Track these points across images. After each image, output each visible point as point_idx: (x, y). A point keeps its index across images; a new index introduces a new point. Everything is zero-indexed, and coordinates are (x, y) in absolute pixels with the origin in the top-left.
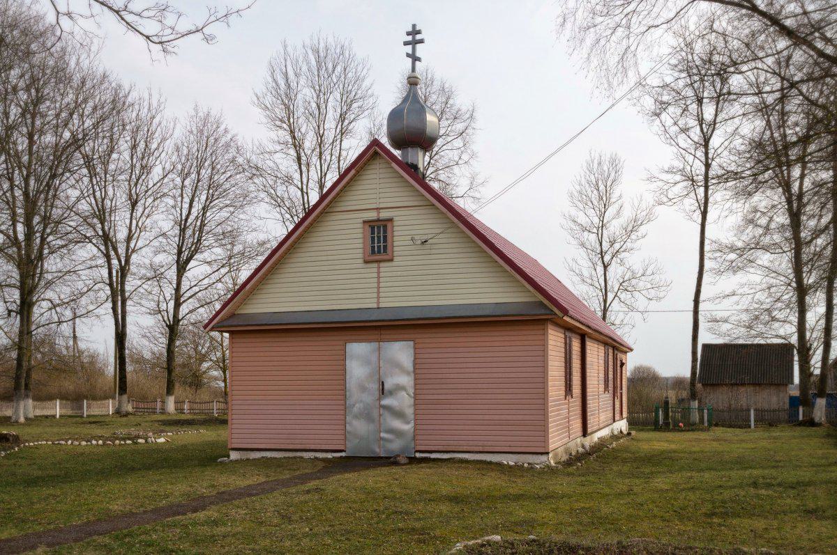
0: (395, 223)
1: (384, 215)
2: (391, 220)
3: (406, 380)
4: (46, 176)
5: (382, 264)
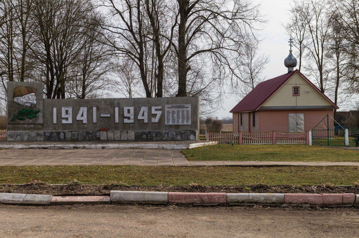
0: (300, 88)
1: (297, 86)
2: (299, 87)
3: (303, 122)
4: (155, 86)
5: (297, 96)
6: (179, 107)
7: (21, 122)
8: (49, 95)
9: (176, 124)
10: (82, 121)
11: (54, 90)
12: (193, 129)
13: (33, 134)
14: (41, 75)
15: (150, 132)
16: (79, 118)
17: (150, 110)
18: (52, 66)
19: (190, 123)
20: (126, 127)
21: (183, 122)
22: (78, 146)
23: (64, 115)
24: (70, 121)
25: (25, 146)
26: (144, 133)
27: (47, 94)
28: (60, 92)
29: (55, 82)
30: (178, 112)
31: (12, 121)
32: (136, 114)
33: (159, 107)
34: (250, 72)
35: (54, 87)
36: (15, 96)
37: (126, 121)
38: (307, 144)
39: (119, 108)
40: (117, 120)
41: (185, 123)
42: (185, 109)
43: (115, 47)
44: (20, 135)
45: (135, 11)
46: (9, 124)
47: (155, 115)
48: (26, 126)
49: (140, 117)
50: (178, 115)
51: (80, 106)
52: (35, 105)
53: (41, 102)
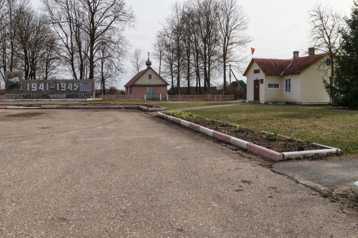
6: (86, 83)
7: (12, 90)
8: (26, 77)
9: (85, 91)
10: (41, 90)
11: (29, 74)
12: (92, 93)
13: (18, 95)
14: (22, 66)
15: (73, 95)
16: (40, 88)
17: (73, 84)
18: (28, 62)
19: (91, 90)
20: (63, 92)
21: (88, 90)
22: (38, 100)
23: (33, 87)
24: (36, 90)
25: (14, 100)
26: (70, 95)
27: (25, 77)
28: (33, 75)
29: (30, 70)
30: (86, 86)
31: (7, 89)
32: (67, 87)
33: (77, 84)
34: (137, 66)
35: (29, 73)
36: (9, 78)
37: (62, 90)
38: (144, 100)
39: (59, 84)
40: (58, 89)
41: (89, 91)
42: (89, 85)
43: (60, 55)
44: (11, 96)
45: (69, 38)
46: (6, 91)
47: (75, 87)
48: (14, 92)
49: (69, 88)
50: (86, 87)
51: (41, 83)
52: (19, 82)
53: (22, 81)
